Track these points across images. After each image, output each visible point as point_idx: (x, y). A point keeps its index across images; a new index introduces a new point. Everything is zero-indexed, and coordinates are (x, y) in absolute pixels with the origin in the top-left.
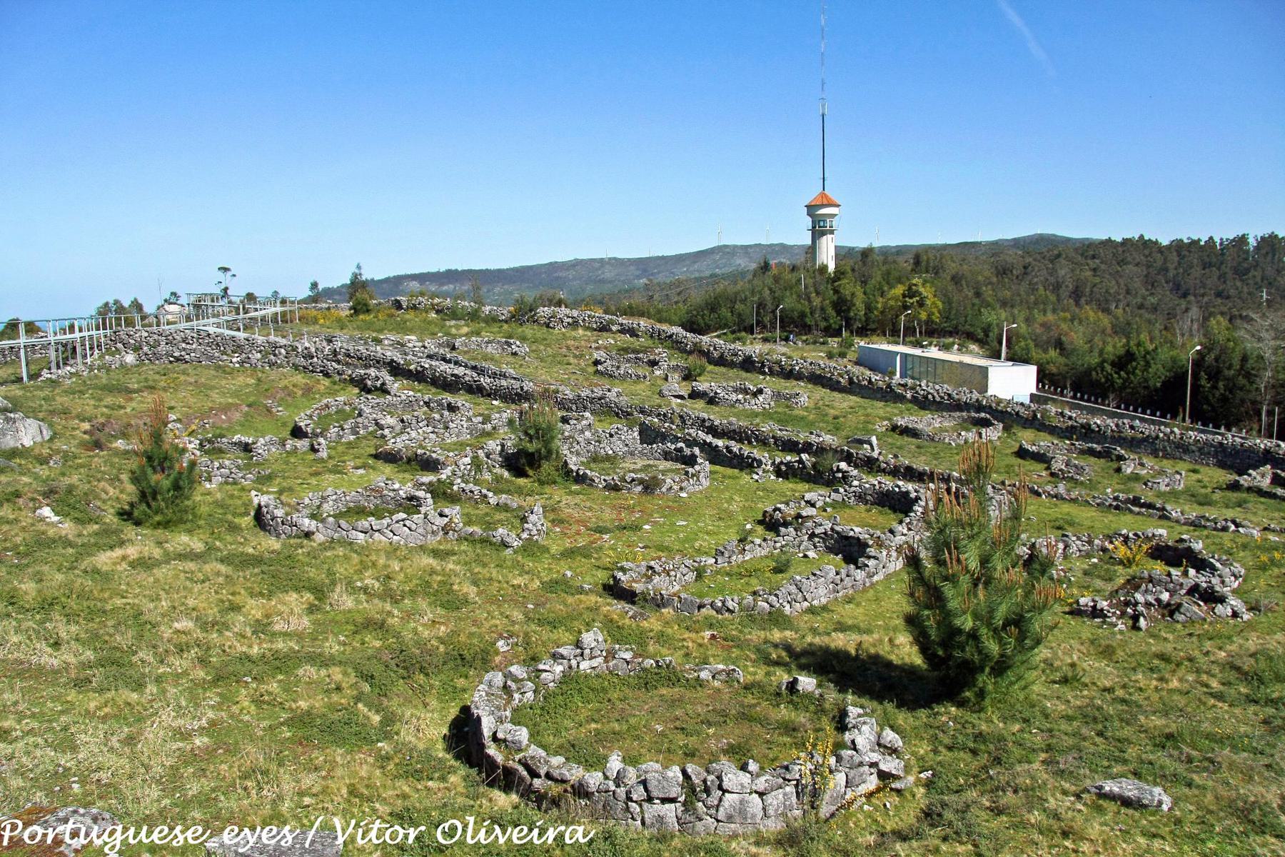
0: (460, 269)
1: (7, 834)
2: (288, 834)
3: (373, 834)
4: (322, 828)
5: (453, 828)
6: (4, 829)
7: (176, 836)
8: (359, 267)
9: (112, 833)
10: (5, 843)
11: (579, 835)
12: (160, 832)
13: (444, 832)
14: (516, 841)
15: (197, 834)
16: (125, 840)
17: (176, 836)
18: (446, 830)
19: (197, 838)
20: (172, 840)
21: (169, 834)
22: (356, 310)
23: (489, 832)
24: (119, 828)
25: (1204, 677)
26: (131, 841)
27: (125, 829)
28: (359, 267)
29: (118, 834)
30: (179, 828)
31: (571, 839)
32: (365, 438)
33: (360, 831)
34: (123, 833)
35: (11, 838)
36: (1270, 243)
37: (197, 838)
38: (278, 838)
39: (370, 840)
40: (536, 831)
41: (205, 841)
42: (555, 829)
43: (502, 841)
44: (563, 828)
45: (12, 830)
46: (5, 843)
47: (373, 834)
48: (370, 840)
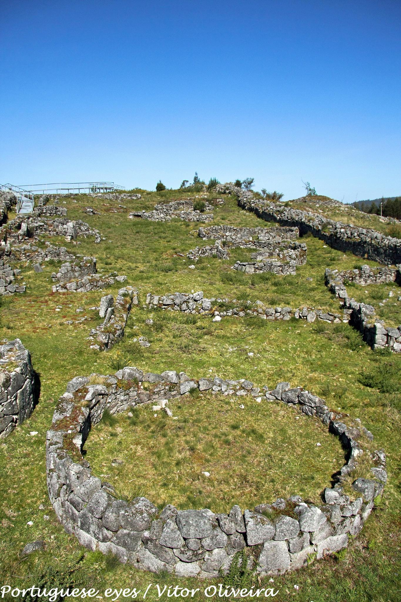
0: (365, 200)
1: (3, 592)
2: (135, 592)
3: (175, 593)
4: (151, 589)
5: (212, 589)
6: (2, 590)
7: (82, 593)
8: (196, 174)
9: (53, 592)
10: (3, 596)
11: (272, 593)
12: (91, 591)
13: (208, 592)
14: (242, 596)
15: (244, 593)
16: (59, 596)
17: (133, 594)
18: (209, 590)
19: (92, 595)
20: (81, 595)
21: (79, 592)
22: (221, 355)
23: (229, 590)
24: (56, 589)
25: (34, 499)
26: (62, 596)
27: (65, 591)
28: (196, 174)
29: (56, 592)
30: (135, 589)
31: (63, 595)
32: (60, 423)
33: (169, 591)
34: (58, 592)
35: (5, 594)
36: (400, 197)
37: (92, 595)
38: (131, 594)
39: (66, 595)
40: (251, 591)
41: (96, 596)
42: (260, 590)
43: (235, 595)
44: (264, 589)
45: (6, 591)
46: (3, 596)
47: (175, 593)
48: (66, 595)
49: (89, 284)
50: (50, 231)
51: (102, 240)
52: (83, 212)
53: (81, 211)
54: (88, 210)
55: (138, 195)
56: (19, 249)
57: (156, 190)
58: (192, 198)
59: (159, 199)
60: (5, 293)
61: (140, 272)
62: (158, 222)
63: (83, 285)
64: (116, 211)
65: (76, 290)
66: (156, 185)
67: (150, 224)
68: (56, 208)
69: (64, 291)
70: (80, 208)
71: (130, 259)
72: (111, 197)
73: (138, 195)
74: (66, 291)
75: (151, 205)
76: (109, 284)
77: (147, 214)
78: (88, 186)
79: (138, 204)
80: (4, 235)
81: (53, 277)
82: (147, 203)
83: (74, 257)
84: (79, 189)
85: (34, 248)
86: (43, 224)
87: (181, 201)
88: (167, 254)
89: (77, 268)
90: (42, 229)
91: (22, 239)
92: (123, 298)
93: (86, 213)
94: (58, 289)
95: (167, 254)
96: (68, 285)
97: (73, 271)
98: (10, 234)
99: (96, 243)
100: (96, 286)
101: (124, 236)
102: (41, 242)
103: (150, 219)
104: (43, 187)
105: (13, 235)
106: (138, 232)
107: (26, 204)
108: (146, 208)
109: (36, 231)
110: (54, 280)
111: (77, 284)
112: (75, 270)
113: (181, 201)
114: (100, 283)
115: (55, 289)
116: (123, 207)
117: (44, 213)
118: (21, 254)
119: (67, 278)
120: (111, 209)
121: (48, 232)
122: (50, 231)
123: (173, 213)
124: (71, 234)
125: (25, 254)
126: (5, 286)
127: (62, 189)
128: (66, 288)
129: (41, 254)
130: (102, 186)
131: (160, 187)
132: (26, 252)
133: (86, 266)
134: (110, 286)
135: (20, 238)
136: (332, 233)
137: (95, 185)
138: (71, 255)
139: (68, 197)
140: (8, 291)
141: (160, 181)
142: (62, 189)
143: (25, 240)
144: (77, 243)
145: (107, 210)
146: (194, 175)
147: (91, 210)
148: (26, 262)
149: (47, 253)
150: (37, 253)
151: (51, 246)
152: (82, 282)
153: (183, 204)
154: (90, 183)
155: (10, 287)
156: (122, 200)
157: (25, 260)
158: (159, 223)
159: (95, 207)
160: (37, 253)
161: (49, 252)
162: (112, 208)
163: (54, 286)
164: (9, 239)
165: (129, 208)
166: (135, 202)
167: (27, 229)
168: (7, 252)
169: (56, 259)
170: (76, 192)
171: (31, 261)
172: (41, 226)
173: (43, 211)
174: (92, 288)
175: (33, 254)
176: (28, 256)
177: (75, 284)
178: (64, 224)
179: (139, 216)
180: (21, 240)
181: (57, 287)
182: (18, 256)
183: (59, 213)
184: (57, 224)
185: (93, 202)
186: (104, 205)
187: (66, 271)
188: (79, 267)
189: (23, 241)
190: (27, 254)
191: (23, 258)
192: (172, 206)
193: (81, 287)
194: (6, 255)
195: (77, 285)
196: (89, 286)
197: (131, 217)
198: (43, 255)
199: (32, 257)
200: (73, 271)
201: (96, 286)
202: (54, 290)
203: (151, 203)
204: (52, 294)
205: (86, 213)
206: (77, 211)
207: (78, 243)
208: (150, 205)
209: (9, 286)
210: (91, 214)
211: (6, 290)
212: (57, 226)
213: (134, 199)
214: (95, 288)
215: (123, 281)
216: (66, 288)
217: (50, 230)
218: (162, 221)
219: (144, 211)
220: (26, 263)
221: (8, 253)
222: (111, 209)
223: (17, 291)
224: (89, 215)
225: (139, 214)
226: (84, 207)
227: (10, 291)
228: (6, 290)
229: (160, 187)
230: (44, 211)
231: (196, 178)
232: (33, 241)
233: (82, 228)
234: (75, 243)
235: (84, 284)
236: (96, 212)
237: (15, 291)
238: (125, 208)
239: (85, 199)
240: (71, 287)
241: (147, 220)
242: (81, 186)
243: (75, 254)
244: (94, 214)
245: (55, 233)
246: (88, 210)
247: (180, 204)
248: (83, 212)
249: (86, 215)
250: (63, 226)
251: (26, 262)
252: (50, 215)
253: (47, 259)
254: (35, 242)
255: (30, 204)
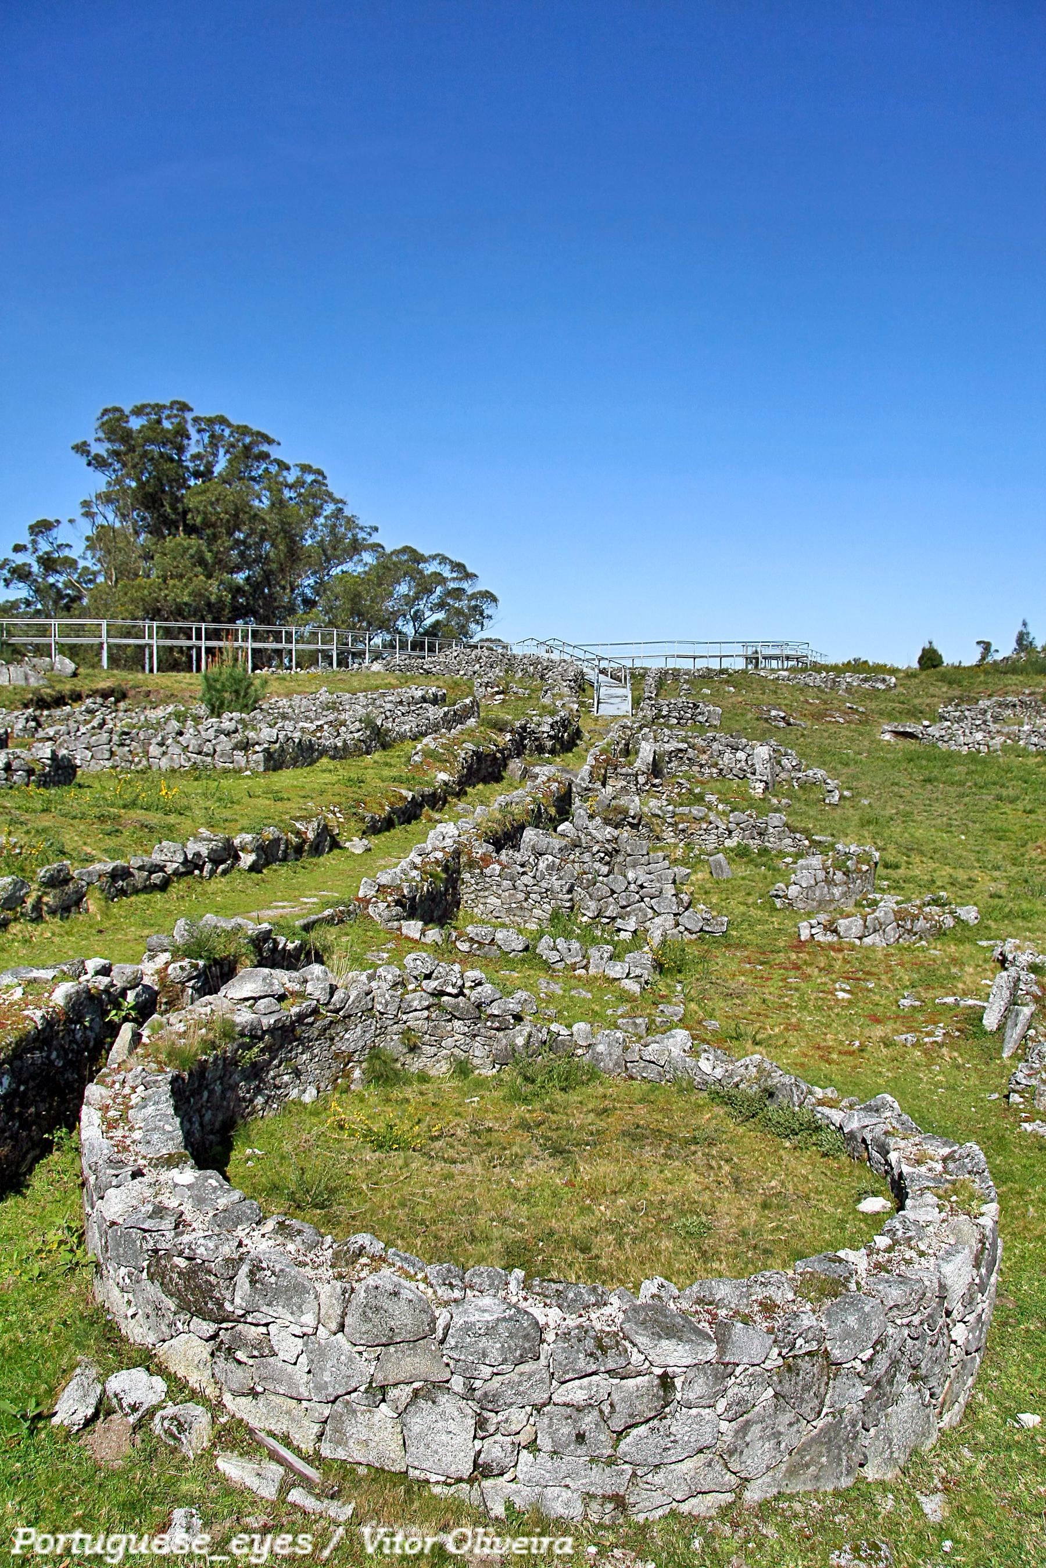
8: (1025, 624)
28: (1025, 624)
49: (895, 924)
50: (701, 766)
51: (842, 797)
52: (757, 719)
53: (750, 716)
54: (773, 713)
55: (888, 677)
56: (660, 813)
57: (915, 665)
58: (1037, 690)
59: (944, 690)
60: (675, 931)
61: (991, 896)
62: (970, 753)
63: (878, 927)
64: (841, 720)
65: (860, 938)
66: (919, 653)
67: (950, 758)
68: (694, 705)
69: (831, 938)
70: (749, 707)
71: (938, 854)
72: (818, 682)
73: (888, 677)
74: (836, 938)
75: (927, 705)
76: (941, 927)
77: (934, 731)
78: (739, 650)
79: (893, 701)
80: (603, 771)
81: (777, 896)
82: (917, 701)
83: (807, 842)
84: (721, 657)
85: (699, 811)
86: (686, 745)
87: (1010, 699)
88: (1040, 847)
89: (839, 876)
90: (681, 758)
91: (646, 783)
92: (1032, 976)
93: (766, 720)
94: (814, 931)
95: (1040, 847)
96: (842, 924)
97: (829, 882)
98: (615, 769)
99: (830, 804)
100: (909, 931)
101: (896, 789)
102: (695, 795)
103: (944, 747)
104: (632, 651)
105: (624, 771)
106: (929, 780)
107: (609, 692)
108: (915, 714)
109: (668, 763)
110: (778, 903)
111: (865, 921)
112: (833, 880)
113: (1010, 699)
114: (921, 924)
115: (807, 931)
116: (857, 710)
117: (663, 717)
118: (663, 824)
119: (813, 900)
120: (828, 712)
121: (697, 768)
122: (701, 766)
123: (998, 732)
124: (765, 778)
125: (676, 824)
126: (675, 915)
127: (678, 656)
128: (835, 931)
129: (717, 827)
130: (776, 652)
131: (930, 659)
132: (676, 819)
133: (860, 870)
134: (945, 934)
135: (642, 779)
136: (403, 774)
137: (759, 649)
138: (798, 836)
139: (707, 676)
140: (681, 928)
141: (930, 643)
142: (678, 656)
143: (654, 786)
144: (780, 802)
145: (819, 716)
146: (1019, 628)
147: (782, 714)
148: (676, 845)
149: (732, 826)
150: (704, 826)
151: (721, 807)
152: (877, 918)
153: (1014, 706)
154: (745, 644)
155: (689, 917)
156: (848, 690)
157: (673, 840)
158: (973, 757)
159: (786, 705)
160: (704, 826)
161: (738, 824)
162: (831, 709)
163: (805, 924)
164: (610, 782)
165: (872, 711)
166: (883, 696)
167: (654, 758)
168: (633, 818)
169: (754, 844)
170: (714, 664)
171: (689, 844)
172: (681, 750)
173: (661, 711)
174: (900, 937)
175: (694, 826)
176: (683, 831)
177: (861, 922)
178: (737, 750)
179: (911, 736)
180: (644, 785)
181: (812, 927)
182: (658, 829)
183: (700, 718)
184: (721, 748)
185: (776, 692)
186: (807, 701)
187: (813, 882)
188: (844, 874)
189: (647, 787)
190: (681, 826)
191: (668, 835)
192: (986, 711)
193: (875, 931)
194: (630, 824)
195: (866, 927)
196: (894, 929)
197: (887, 737)
198: (721, 830)
199: (692, 834)
200: (829, 882)
201: (909, 931)
202: (805, 935)
203: (928, 701)
204: (799, 945)
205: (766, 720)
206: (742, 715)
207: (784, 801)
208: (924, 706)
209: (686, 913)
210: (782, 724)
211: (677, 925)
212: (721, 753)
213: (878, 690)
214: (906, 935)
215: (976, 922)
216: (835, 931)
217: (703, 762)
218: (979, 752)
219: (926, 723)
220: (675, 848)
221: (635, 821)
222: (828, 712)
223: (707, 928)
224: (776, 727)
225: (909, 730)
226: (758, 706)
227: (686, 929)
228: (677, 925)
229: (930, 659)
230: (664, 713)
231: (1021, 638)
232: (671, 791)
233: (785, 762)
234: (775, 801)
235: (881, 924)
236: (792, 721)
237: (701, 930)
238: (863, 713)
239: (754, 686)
240: (848, 929)
241: (934, 745)
242: (726, 650)
243: (807, 833)
244: (789, 724)
245: (715, 770)
246: (773, 713)
247: (1007, 706)
248: (757, 719)
249: (766, 725)
250: (734, 754)
251: (676, 845)
252: (678, 723)
253: (729, 843)
254: (679, 794)
255: (621, 691)
